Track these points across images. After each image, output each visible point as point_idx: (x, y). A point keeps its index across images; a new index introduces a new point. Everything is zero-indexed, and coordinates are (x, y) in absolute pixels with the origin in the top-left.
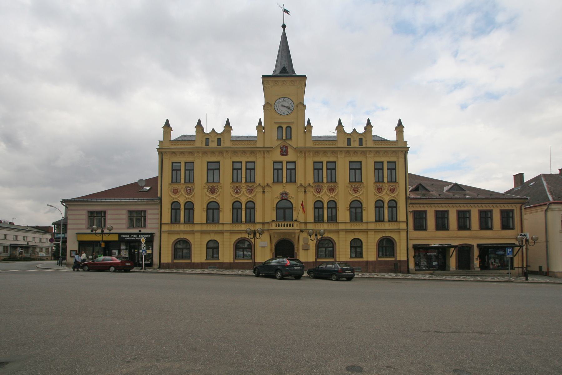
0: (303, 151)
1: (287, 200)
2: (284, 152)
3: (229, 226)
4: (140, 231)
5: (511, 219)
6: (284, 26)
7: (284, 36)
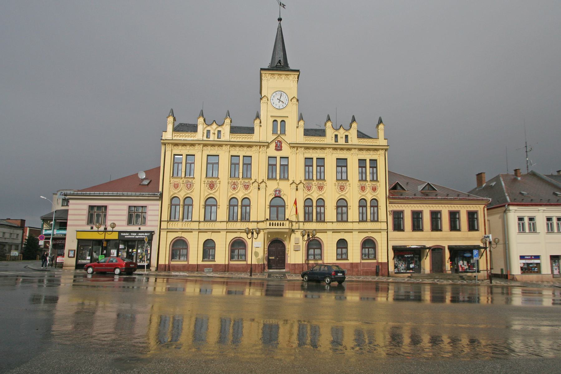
1: (280, 197)
2: (279, 148)
4: (140, 229)
6: (280, 20)
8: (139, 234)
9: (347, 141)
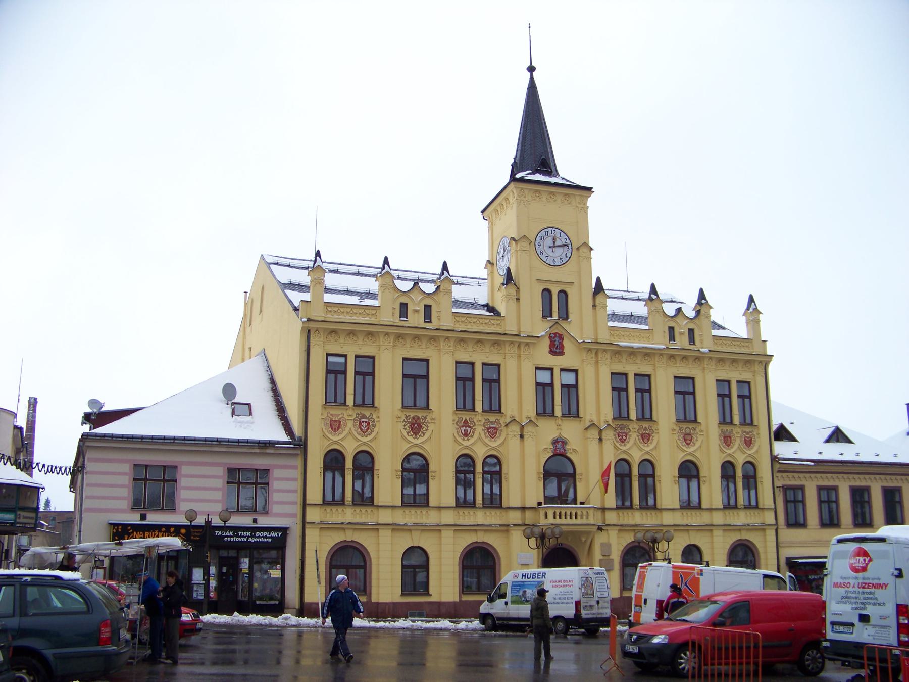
0: (595, 348)
1: (563, 455)
2: (557, 349)
3: (389, 512)
4: (255, 521)
5: (866, 505)
6: (531, 69)
7: (532, 89)
8: (258, 534)
9: (428, 317)
